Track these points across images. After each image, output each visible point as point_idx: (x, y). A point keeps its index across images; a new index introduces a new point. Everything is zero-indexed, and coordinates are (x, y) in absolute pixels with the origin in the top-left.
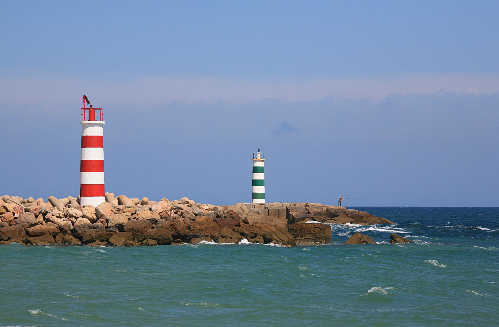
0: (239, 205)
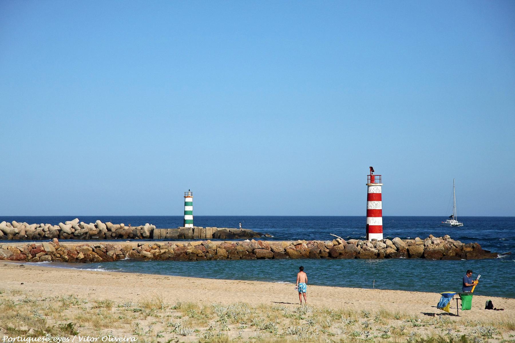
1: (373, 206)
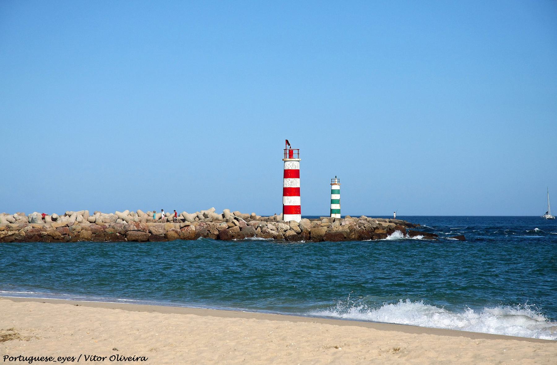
0: (35, 213)
1: (288, 184)
